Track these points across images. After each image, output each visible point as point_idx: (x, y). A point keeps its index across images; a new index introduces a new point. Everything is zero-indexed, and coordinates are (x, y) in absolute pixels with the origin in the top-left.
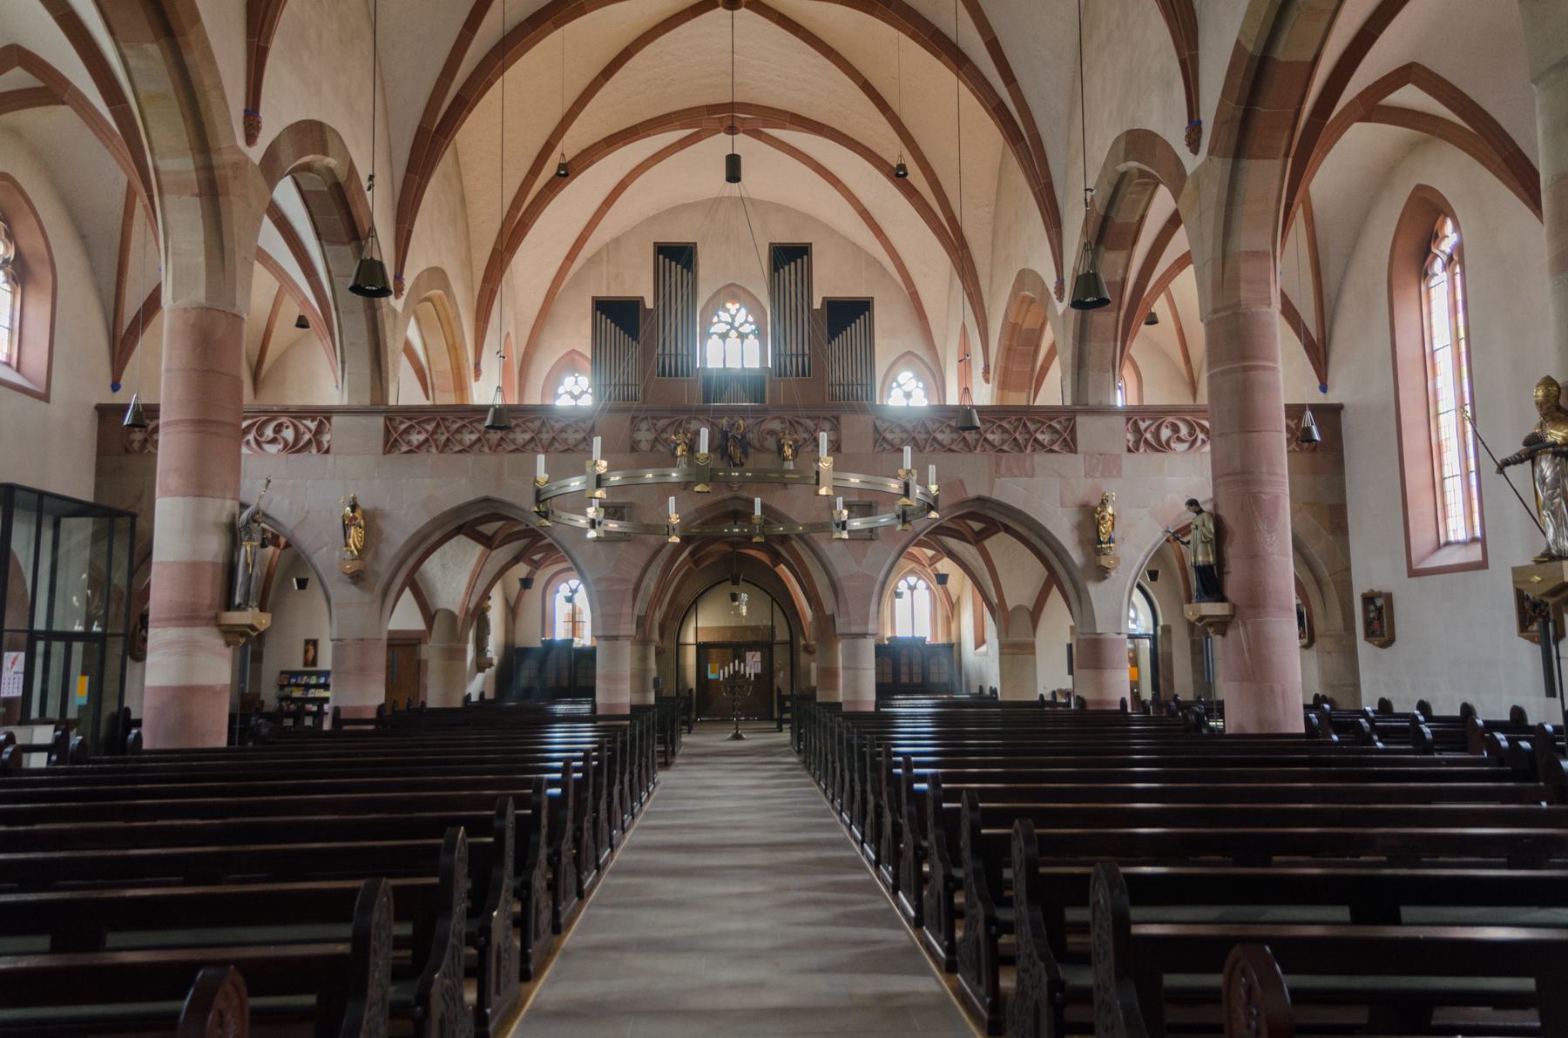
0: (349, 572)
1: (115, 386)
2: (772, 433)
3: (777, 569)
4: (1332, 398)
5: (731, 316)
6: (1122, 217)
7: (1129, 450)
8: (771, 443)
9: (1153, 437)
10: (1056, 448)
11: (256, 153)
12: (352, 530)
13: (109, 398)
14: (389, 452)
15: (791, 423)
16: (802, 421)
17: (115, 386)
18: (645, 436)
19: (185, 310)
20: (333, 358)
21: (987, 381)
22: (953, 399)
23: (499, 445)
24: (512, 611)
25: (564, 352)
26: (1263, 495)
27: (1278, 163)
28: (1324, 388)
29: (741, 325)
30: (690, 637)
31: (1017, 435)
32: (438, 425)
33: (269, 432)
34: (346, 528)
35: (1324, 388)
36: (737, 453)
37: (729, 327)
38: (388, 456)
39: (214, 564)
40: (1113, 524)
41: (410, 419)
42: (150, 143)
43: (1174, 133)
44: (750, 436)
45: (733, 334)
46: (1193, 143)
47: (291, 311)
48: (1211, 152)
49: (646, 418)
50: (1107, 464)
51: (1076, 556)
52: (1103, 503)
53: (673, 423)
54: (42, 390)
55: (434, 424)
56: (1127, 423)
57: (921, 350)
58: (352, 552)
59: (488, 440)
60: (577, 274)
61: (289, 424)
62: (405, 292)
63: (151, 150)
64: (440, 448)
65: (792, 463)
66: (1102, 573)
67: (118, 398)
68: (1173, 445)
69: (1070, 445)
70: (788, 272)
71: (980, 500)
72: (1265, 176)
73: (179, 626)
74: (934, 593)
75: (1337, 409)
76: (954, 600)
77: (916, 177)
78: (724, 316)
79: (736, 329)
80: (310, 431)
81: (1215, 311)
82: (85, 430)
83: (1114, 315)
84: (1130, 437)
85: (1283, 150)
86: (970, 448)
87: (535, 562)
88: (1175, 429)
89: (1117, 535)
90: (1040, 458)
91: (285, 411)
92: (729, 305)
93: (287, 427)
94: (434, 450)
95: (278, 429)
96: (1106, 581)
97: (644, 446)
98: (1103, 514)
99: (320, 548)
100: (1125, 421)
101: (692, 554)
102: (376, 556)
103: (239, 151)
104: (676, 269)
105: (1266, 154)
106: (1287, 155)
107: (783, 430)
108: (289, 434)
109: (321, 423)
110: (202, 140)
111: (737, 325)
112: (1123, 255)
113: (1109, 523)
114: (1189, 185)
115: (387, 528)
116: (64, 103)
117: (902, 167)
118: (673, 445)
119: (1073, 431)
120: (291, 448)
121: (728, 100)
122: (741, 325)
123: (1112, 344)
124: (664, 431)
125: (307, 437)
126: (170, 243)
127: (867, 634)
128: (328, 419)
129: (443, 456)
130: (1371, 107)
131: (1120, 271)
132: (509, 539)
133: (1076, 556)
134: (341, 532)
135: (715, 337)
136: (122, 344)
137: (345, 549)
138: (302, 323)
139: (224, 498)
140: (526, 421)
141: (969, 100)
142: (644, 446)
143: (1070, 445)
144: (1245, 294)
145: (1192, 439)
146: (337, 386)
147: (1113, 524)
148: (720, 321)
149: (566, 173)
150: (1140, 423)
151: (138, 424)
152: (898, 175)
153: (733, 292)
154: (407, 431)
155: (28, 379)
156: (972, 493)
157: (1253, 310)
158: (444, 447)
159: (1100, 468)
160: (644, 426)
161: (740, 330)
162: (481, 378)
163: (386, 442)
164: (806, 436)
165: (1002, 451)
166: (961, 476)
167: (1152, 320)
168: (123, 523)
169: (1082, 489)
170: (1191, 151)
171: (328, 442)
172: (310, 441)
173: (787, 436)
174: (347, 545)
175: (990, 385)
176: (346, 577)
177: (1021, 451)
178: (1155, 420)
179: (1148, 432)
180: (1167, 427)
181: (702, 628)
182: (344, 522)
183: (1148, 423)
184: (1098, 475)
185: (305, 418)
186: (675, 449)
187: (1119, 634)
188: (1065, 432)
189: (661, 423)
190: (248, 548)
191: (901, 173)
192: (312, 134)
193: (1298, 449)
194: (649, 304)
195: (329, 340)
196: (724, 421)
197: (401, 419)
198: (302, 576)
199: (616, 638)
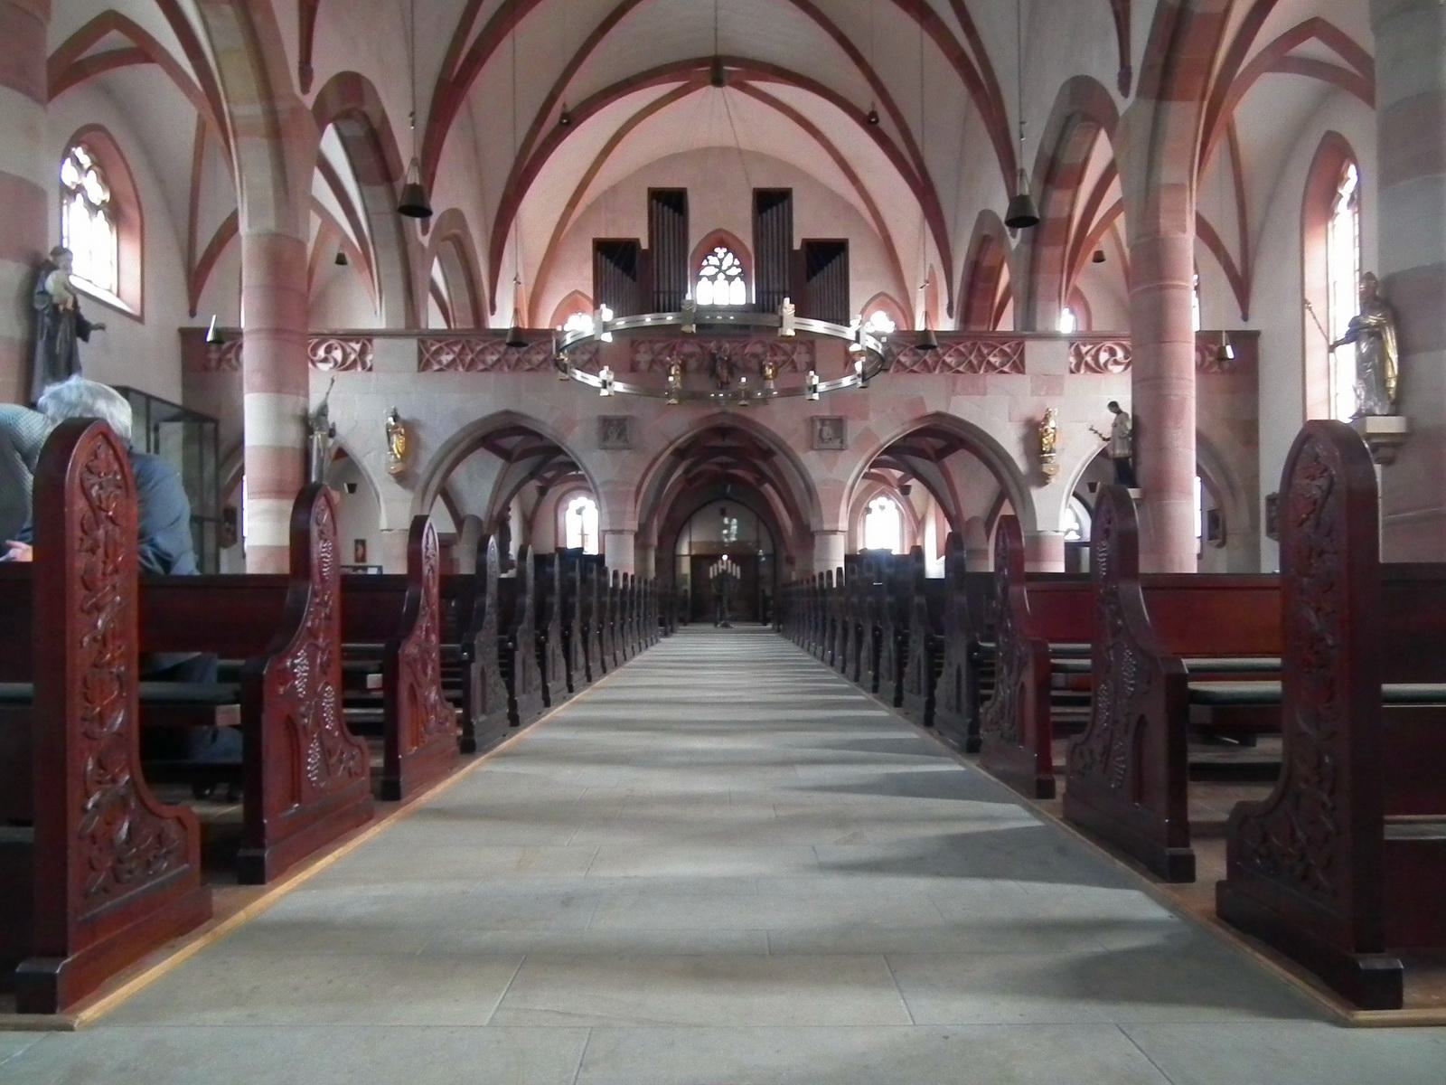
0: (394, 472)
1: (193, 313)
2: (755, 355)
3: (762, 489)
4: (1251, 326)
5: (719, 259)
6: (1067, 159)
7: (1072, 372)
8: (754, 364)
9: (1092, 360)
10: (1006, 369)
11: (309, 101)
12: (394, 438)
13: (188, 323)
14: (423, 370)
15: (772, 348)
16: (782, 345)
17: (193, 313)
18: (643, 358)
19: (259, 235)
20: (371, 288)
21: (951, 316)
22: (920, 326)
23: (516, 365)
24: (529, 524)
25: (569, 292)
26: (1172, 397)
27: (1196, 103)
28: (1245, 317)
29: (729, 268)
30: (684, 549)
31: (972, 358)
32: (463, 348)
33: (321, 353)
34: (389, 435)
35: (1245, 317)
36: (724, 373)
37: (717, 270)
38: (423, 373)
39: (294, 448)
40: (1054, 436)
41: (440, 341)
42: (225, 91)
43: (1109, 80)
44: (734, 358)
45: (721, 276)
46: (1124, 86)
47: (334, 249)
48: (1139, 94)
49: (643, 342)
50: (1051, 384)
51: (1022, 465)
52: (1046, 419)
53: (668, 345)
54: (137, 312)
55: (460, 347)
56: (1071, 346)
57: (892, 292)
58: (395, 455)
59: (507, 361)
60: (577, 222)
61: (337, 345)
62: (431, 230)
63: (227, 97)
64: (466, 366)
65: (772, 382)
66: (1043, 479)
67: (197, 323)
68: (1110, 367)
69: (1019, 368)
70: (772, 214)
71: (938, 415)
72: (1183, 117)
73: (270, 498)
74: (903, 514)
75: (1254, 336)
76: (920, 517)
77: (886, 123)
78: (713, 260)
79: (724, 272)
80: (355, 350)
81: (1138, 237)
82: (172, 348)
83: (1061, 248)
84: (1072, 360)
85: (1199, 92)
86: (928, 369)
87: (546, 479)
88: (1112, 352)
89: (1056, 446)
90: (993, 378)
91: (334, 335)
92: (717, 250)
93: (336, 349)
94: (460, 369)
95: (329, 350)
96: (1047, 486)
97: (643, 366)
98: (1046, 427)
99: (369, 453)
100: (1069, 345)
101: (686, 472)
102: (416, 459)
103: (297, 99)
104: (668, 213)
105: (1185, 96)
106: (1203, 98)
107: (765, 353)
108: (338, 354)
109: (364, 345)
110: (268, 93)
111: (724, 268)
112: (1069, 193)
113: (1052, 435)
114: (1121, 124)
115: (423, 435)
116: (152, 61)
117: (873, 114)
118: (668, 366)
119: (1022, 355)
120: (340, 366)
121: (712, 53)
122: (729, 268)
123: (1059, 275)
124: (659, 354)
125: (353, 357)
126: (244, 178)
127: (837, 531)
128: (370, 341)
129: (469, 373)
130: (1281, 57)
131: (1067, 209)
132: (525, 454)
133: (1022, 465)
134: (385, 438)
135: (704, 279)
136: (196, 276)
137: (389, 453)
138: (341, 260)
139: (298, 394)
140: (540, 344)
141: (931, 49)
142: (643, 366)
143: (1019, 368)
144: (1165, 222)
145: (1127, 361)
146: (376, 313)
147: (1054, 436)
148: (708, 265)
149: (570, 122)
150: (1082, 347)
151: (218, 340)
152: (869, 122)
153: (720, 239)
154: (438, 352)
155: (127, 304)
156: (930, 410)
157: (1171, 236)
158: (470, 366)
159: (1045, 388)
160: (642, 348)
161: (728, 273)
162: (497, 312)
163: (420, 361)
164: (783, 358)
165: (958, 372)
166: (922, 393)
167: (1099, 258)
168: (209, 427)
169: (1029, 406)
170: (1123, 94)
171: (371, 361)
172: (355, 362)
173: (769, 358)
174: (391, 450)
175: (953, 320)
176: (392, 478)
177: (975, 372)
178: (1095, 344)
179: (1088, 354)
180: (1105, 351)
181: (696, 543)
182: (387, 429)
183: (1089, 347)
184: (1043, 393)
185: (351, 340)
186: (670, 369)
187: (1057, 531)
188: (1015, 354)
189: (658, 346)
190: (319, 436)
191: (873, 120)
192: (351, 86)
193: (1219, 371)
194: (644, 245)
195: (367, 271)
196: (712, 345)
197: (431, 341)
198: (352, 482)
199: (621, 532)
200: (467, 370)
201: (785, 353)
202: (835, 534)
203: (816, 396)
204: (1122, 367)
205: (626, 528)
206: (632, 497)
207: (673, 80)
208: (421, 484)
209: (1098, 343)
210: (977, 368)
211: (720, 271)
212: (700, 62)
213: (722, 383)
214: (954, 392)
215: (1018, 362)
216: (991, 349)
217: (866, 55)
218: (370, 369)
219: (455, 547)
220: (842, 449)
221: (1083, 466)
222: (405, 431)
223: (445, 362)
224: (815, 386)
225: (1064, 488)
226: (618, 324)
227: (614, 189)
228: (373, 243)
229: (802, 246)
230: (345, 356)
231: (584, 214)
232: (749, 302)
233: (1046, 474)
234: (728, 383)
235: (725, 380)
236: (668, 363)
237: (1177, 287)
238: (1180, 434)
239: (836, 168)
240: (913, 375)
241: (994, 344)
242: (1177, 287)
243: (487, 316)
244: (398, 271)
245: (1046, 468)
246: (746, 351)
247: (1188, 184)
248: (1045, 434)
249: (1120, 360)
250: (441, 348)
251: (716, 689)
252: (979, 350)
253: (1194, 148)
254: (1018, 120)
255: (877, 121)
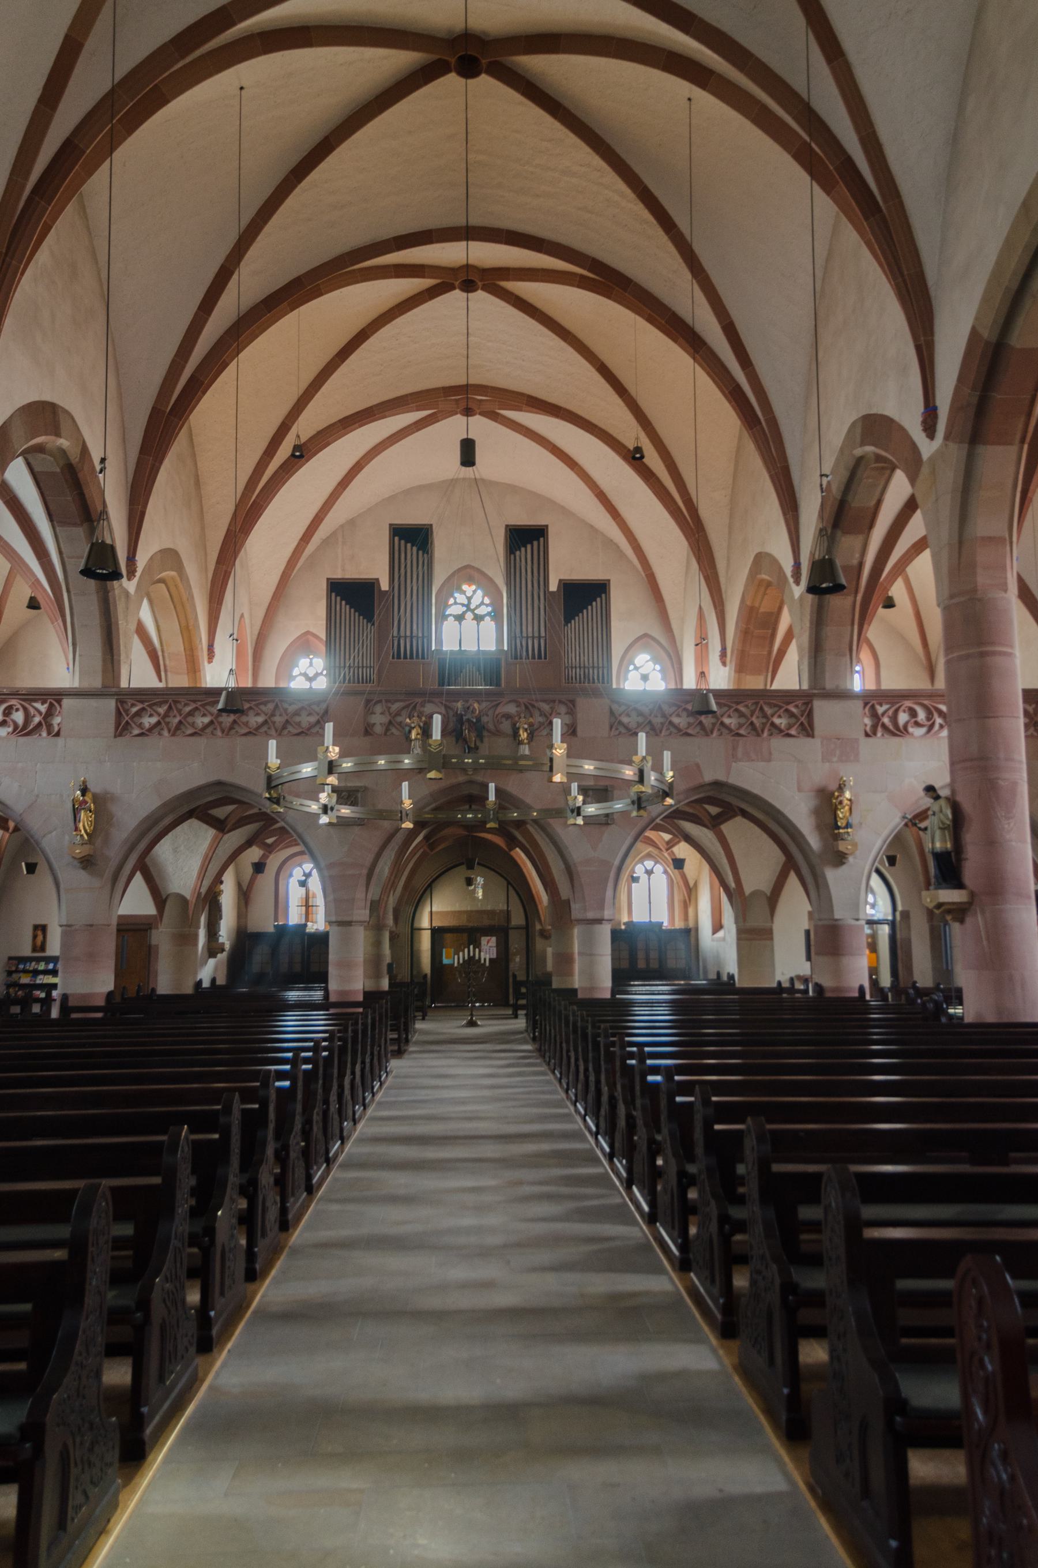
2: (507, 716)
3: (512, 853)
6: (859, 500)
7: (867, 735)
8: (506, 726)
9: (891, 721)
10: (793, 732)
14: (120, 735)
15: (527, 707)
21: (724, 664)
22: (690, 682)
23: (231, 728)
24: (245, 895)
26: (1001, 783)
27: (1014, 449)
32: (170, 707)
34: (75, 812)
37: (465, 609)
41: (142, 702)
43: (912, 422)
45: (469, 616)
46: (929, 429)
48: (947, 437)
49: (380, 701)
51: (814, 841)
52: (841, 788)
53: (407, 706)
55: (166, 707)
57: (657, 632)
58: (82, 836)
61: (19, 706)
62: (138, 574)
64: (173, 729)
65: (527, 746)
68: (911, 730)
69: (807, 729)
70: (525, 554)
76: (691, 884)
77: (653, 459)
78: (461, 598)
79: (473, 611)
80: (40, 713)
81: (952, 596)
83: (850, 599)
84: (868, 721)
85: (1018, 437)
86: (707, 732)
88: (913, 713)
89: (854, 820)
90: (778, 743)
91: (15, 694)
92: (465, 587)
93: (17, 710)
94: (166, 733)
97: (378, 729)
98: (840, 798)
101: (427, 838)
104: (412, 550)
105: (1003, 440)
106: (1022, 441)
108: (19, 717)
109: (51, 705)
111: (472, 606)
112: (860, 538)
114: (925, 471)
115: (116, 810)
117: (638, 449)
118: (407, 729)
119: (810, 715)
123: (849, 628)
124: (398, 714)
125: (37, 719)
127: (603, 920)
128: (59, 702)
131: (857, 555)
133: (814, 841)
135: (451, 619)
138: (33, 604)
142: (378, 729)
143: (807, 729)
146: (68, 669)
148: (456, 603)
149: (301, 454)
150: (878, 707)
152: (634, 458)
153: (469, 573)
156: (708, 777)
162: (215, 660)
163: (118, 724)
164: (541, 719)
165: (738, 735)
167: (889, 604)
169: (820, 774)
172: (40, 724)
174: (77, 829)
176: (76, 863)
177: (758, 735)
178: (893, 704)
180: (904, 711)
181: (438, 913)
185: (35, 701)
186: (410, 732)
187: (857, 920)
188: (802, 716)
189: (395, 707)
191: (638, 456)
194: (385, 586)
197: (132, 701)
199: (349, 923)
200: (173, 735)
201: (542, 714)
202: (601, 923)
203: (580, 821)
204: (923, 730)
205: (355, 919)
206: (363, 881)
207: (419, 409)
208: (108, 873)
209: (898, 703)
210: (759, 730)
211: (469, 609)
212: (449, 391)
213: (469, 748)
214: (734, 757)
215: (806, 724)
216: (776, 709)
217: (632, 390)
218: (58, 734)
219: (154, 931)
220: (607, 824)
221: (885, 842)
222: (95, 808)
223: (147, 726)
224: (579, 808)
225: (864, 869)
226: (304, 770)
227: (352, 523)
228: (68, 591)
229: (559, 587)
230: (28, 718)
231: (318, 549)
232: (500, 648)
233: (842, 852)
234: (477, 748)
235: (473, 745)
236: (407, 725)
237: (994, 653)
238: (1012, 825)
239: (595, 501)
240: (688, 739)
241: (780, 704)
242: (994, 653)
243: (204, 666)
244: (95, 621)
245: (842, 846)
246: (497, 712)
247: (1008, 538)
248: (839, 807)
249: (921, 722)
250: (143, 709)
251: (510, 568)
252: (761, 709)
253: (1014, 496)
254: (819, 474)
255: (642, 457)
